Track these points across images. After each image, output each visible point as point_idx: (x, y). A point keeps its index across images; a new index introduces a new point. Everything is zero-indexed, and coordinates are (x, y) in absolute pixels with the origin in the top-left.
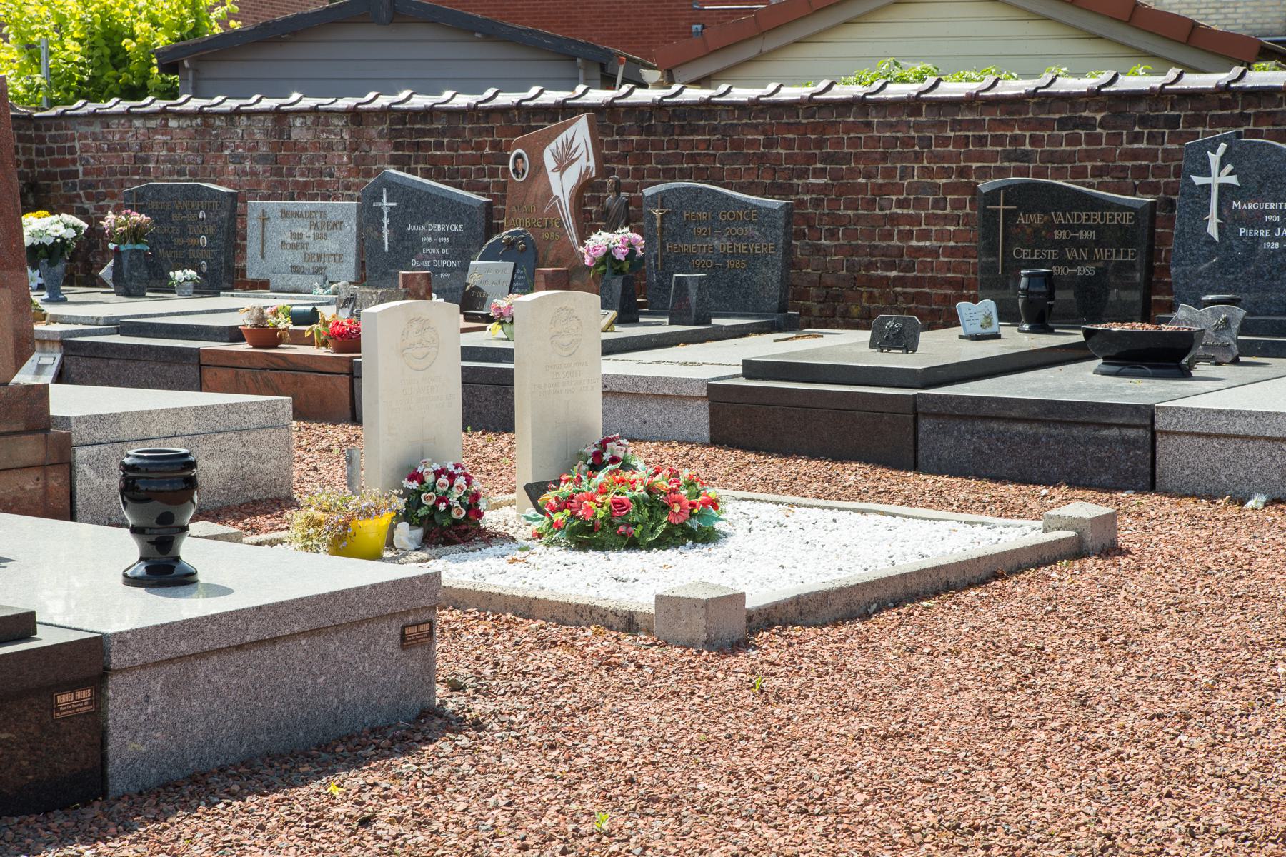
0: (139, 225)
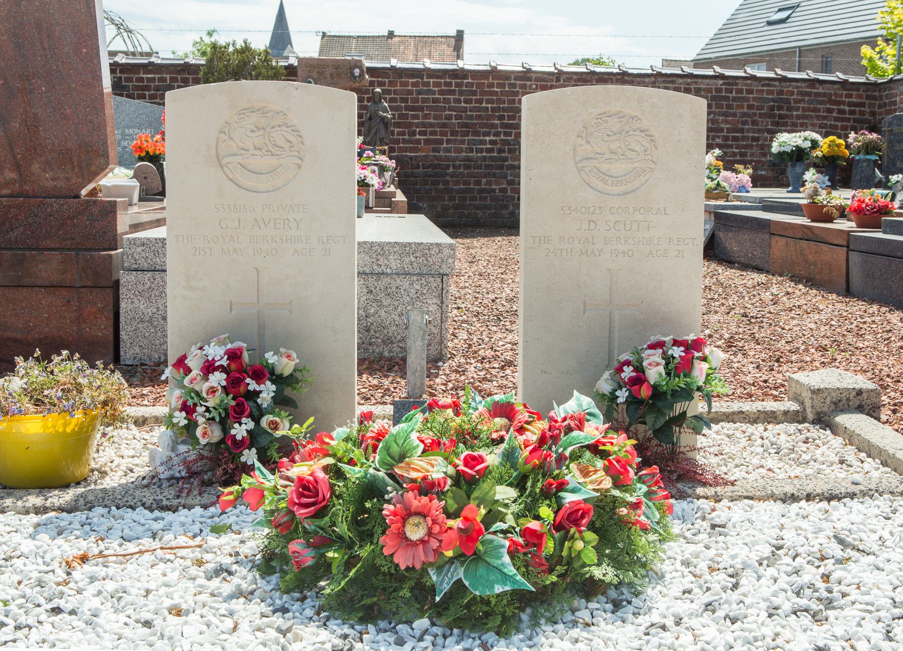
0: (871, 141)
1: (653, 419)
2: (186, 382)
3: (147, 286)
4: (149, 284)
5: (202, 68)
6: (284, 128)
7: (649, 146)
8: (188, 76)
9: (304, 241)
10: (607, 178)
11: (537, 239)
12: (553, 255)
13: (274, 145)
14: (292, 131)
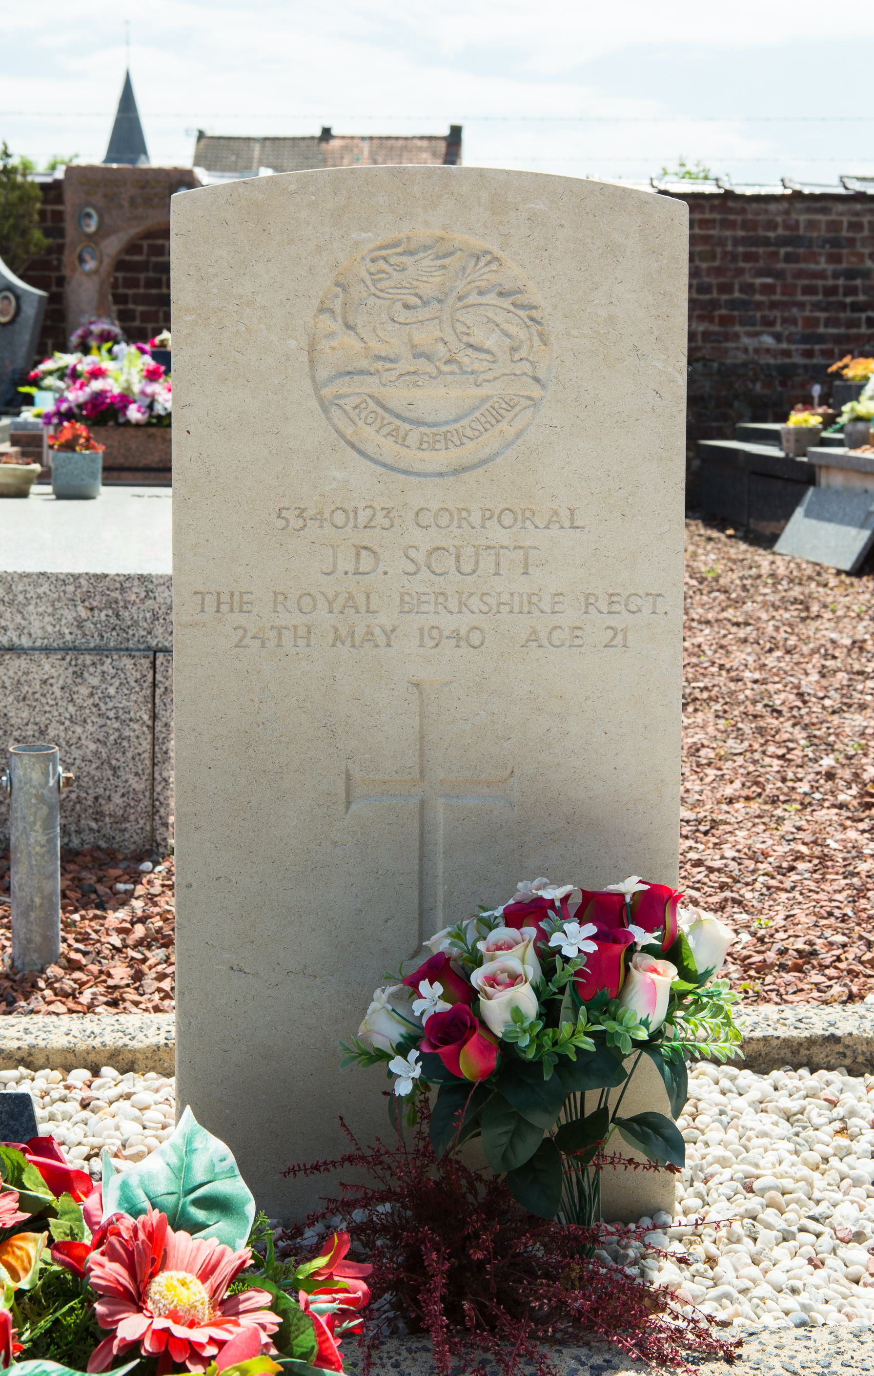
1: (505, 1140)
7: (523, 334)
10: (408, 427)
11: (210, 600)
12: (257, 643)
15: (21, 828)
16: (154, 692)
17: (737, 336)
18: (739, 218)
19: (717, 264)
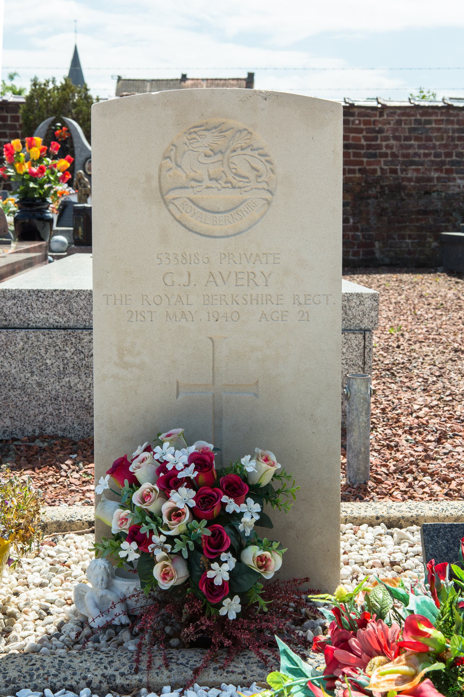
2: (136, 498)
3: (20, 346)
4: (22, 343)
5: (21, 106)
6: (248, 151)
8: (6, 114)
9: (275, 302)
13: (235, 174)
14: (260, 155)
15: (355, 414)
16: (364, 351)
17: (454, 179)
18: (455, 119)
19: (444, 142)
